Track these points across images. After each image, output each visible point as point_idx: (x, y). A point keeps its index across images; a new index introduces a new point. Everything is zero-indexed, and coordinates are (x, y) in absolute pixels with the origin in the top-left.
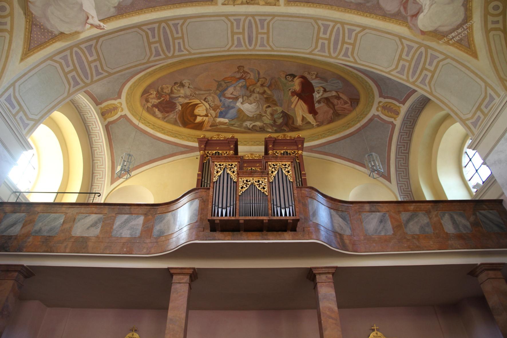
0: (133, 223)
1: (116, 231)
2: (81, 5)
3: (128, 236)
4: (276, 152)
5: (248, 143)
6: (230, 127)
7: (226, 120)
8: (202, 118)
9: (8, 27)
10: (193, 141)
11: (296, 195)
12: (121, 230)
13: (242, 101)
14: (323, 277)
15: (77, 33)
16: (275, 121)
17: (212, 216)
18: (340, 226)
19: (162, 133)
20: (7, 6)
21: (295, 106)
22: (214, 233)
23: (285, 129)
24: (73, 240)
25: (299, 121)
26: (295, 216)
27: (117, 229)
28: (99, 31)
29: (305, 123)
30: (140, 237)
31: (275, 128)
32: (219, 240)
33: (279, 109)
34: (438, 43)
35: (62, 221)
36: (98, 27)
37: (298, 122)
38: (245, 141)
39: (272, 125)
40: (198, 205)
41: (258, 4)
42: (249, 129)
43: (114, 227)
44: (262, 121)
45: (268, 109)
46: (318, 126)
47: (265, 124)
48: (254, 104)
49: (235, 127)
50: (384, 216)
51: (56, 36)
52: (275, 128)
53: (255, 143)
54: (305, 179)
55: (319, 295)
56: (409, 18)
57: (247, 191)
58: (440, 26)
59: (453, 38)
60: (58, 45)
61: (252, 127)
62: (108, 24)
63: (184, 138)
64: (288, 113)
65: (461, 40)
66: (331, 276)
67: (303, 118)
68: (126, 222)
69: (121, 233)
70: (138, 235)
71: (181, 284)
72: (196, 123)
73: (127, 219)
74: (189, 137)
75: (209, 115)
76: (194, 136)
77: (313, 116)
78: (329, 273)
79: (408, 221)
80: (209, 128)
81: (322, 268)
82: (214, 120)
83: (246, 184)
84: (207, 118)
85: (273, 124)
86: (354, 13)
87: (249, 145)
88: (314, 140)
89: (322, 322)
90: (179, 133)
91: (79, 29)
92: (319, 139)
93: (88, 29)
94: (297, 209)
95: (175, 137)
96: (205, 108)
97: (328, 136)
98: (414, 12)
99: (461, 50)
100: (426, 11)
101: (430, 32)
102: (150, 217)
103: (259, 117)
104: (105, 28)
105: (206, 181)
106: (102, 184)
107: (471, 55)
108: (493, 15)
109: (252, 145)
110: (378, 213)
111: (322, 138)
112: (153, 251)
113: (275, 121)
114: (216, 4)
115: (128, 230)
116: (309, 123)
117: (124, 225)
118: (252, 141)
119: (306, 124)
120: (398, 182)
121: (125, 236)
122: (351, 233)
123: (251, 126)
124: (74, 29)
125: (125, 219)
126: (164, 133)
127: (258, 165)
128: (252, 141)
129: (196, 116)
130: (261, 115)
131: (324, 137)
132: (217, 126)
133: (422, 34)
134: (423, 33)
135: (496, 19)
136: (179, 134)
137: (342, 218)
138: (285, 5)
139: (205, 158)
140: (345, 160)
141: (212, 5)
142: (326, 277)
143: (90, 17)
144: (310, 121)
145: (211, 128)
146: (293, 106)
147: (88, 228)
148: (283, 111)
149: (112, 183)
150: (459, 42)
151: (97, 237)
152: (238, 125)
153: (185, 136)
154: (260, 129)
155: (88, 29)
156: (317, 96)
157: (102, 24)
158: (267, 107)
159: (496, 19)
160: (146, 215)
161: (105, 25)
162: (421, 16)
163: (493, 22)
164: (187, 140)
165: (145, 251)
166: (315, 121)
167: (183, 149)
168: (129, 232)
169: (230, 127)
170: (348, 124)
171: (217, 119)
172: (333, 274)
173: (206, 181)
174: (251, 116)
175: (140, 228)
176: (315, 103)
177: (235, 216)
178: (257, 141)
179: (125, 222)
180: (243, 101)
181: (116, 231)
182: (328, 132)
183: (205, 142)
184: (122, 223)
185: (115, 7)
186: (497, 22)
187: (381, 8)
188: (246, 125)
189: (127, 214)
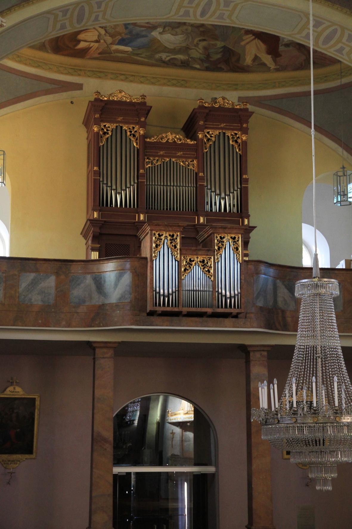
0: (43, 285)
1: (24, 296)
3: (40, 303)
4: (208, 133)
5: (159, 81)
6: (132, 57)
7: (129, 49)
8: (88, 44)
10: (66, 74)
11: (234, 227)
12: (30, 295)
13: (162, 31)
14: (258, 355)
16: (208, 56)
17: (153, 306)
18: (285, 300)
19: (16, 61)
21: (248, 43)
22: (152, 317)
23: (223, 67)
25: (248, 60)
26: (240, 308)
27: (24, 294)
29: (256, 64)
31: (206, 65)
32: (157, 325)
33: (220, 44)
37: (246, 61)
38: (153, 78)
39: (202, 60)
40: (131, 280)
43: (20, 290)
44: (189, 55)
45: (201, 42)
46: (277, 70)
47: (191, 58)
48: (182, 36)
49: (140, 57)
52: (206, 65)
53: (169, 81)
54: (247, 188)
55: (251, 374)
57: (190, 273)
61: (169, 60)
63: (52, 69)
64: (234, 49)
67: (256, 58)
68: (34, 283)
69: (31, 299)
70: (52, 302)
71: (106, 359)
72: (75, 49)
73: (33, 280)
74: (61, 67)
75: (102, 41)
76: (70, 65)
77: (272, 57)
78: (263, 351)
80: (96, 55)
81: (257, 346)
82: (108, 47)
83: (190, 264)
84: (96, 45)
85: (205, 59)
87: (160, 85)
88: (265, 88)
89: (251, 403)
90: (44, 61)
92: (274, 87)
94: (243, 300)
95: (38, 67)
96: (97, 33)
97: (291, 85)
102: (63, 277)
103: (185, 50)
104: (4, 24)
109: (164, 85)
111: (279, 87)
113: (208, 56)
115: (38, 294)
116: (264, 64)
117: (31, 288)
118: (164, 79)
119: (258, 65)
121: (36, 303)
122: (295, 308)
123: (168, 58)
125: (32, 280)
126: (20, 62)
127: (179, 154)
128: (164, 79)
129: (79, 41)
130: (188, 48)
132: (112, 53)
136: (44, 63)
137: (288, 289)
139: (101, 137)
142: (261, 354)
144: (266, 62)
145: (100, 56)
146: (243, 43)
148: (225, 46)
152: (146, 55)
153: (54, 65)
154: (182, 63)
156: (295, 424)
158: (200, 41)
160: (57, 274)
161: (4, 20)
164: (56, 72)
165: (64, 323)
166: (274, 64)
167: (49, 86)
169: (132, 57)
170: (326, 77)
171: (113, 45)
172: (268, 351)
173: (105, 182)
174: (172, 48)
175: (53, 291)
176: (280, 45)
177: (178, 306)
178: (173, 79)
179: (32, 283)
180: (163, 31)
181: (24, 296)
182: (292, 81)
183: (101, 108)
184: (29, 285)
188: (161, 57)
189: (33, 272)
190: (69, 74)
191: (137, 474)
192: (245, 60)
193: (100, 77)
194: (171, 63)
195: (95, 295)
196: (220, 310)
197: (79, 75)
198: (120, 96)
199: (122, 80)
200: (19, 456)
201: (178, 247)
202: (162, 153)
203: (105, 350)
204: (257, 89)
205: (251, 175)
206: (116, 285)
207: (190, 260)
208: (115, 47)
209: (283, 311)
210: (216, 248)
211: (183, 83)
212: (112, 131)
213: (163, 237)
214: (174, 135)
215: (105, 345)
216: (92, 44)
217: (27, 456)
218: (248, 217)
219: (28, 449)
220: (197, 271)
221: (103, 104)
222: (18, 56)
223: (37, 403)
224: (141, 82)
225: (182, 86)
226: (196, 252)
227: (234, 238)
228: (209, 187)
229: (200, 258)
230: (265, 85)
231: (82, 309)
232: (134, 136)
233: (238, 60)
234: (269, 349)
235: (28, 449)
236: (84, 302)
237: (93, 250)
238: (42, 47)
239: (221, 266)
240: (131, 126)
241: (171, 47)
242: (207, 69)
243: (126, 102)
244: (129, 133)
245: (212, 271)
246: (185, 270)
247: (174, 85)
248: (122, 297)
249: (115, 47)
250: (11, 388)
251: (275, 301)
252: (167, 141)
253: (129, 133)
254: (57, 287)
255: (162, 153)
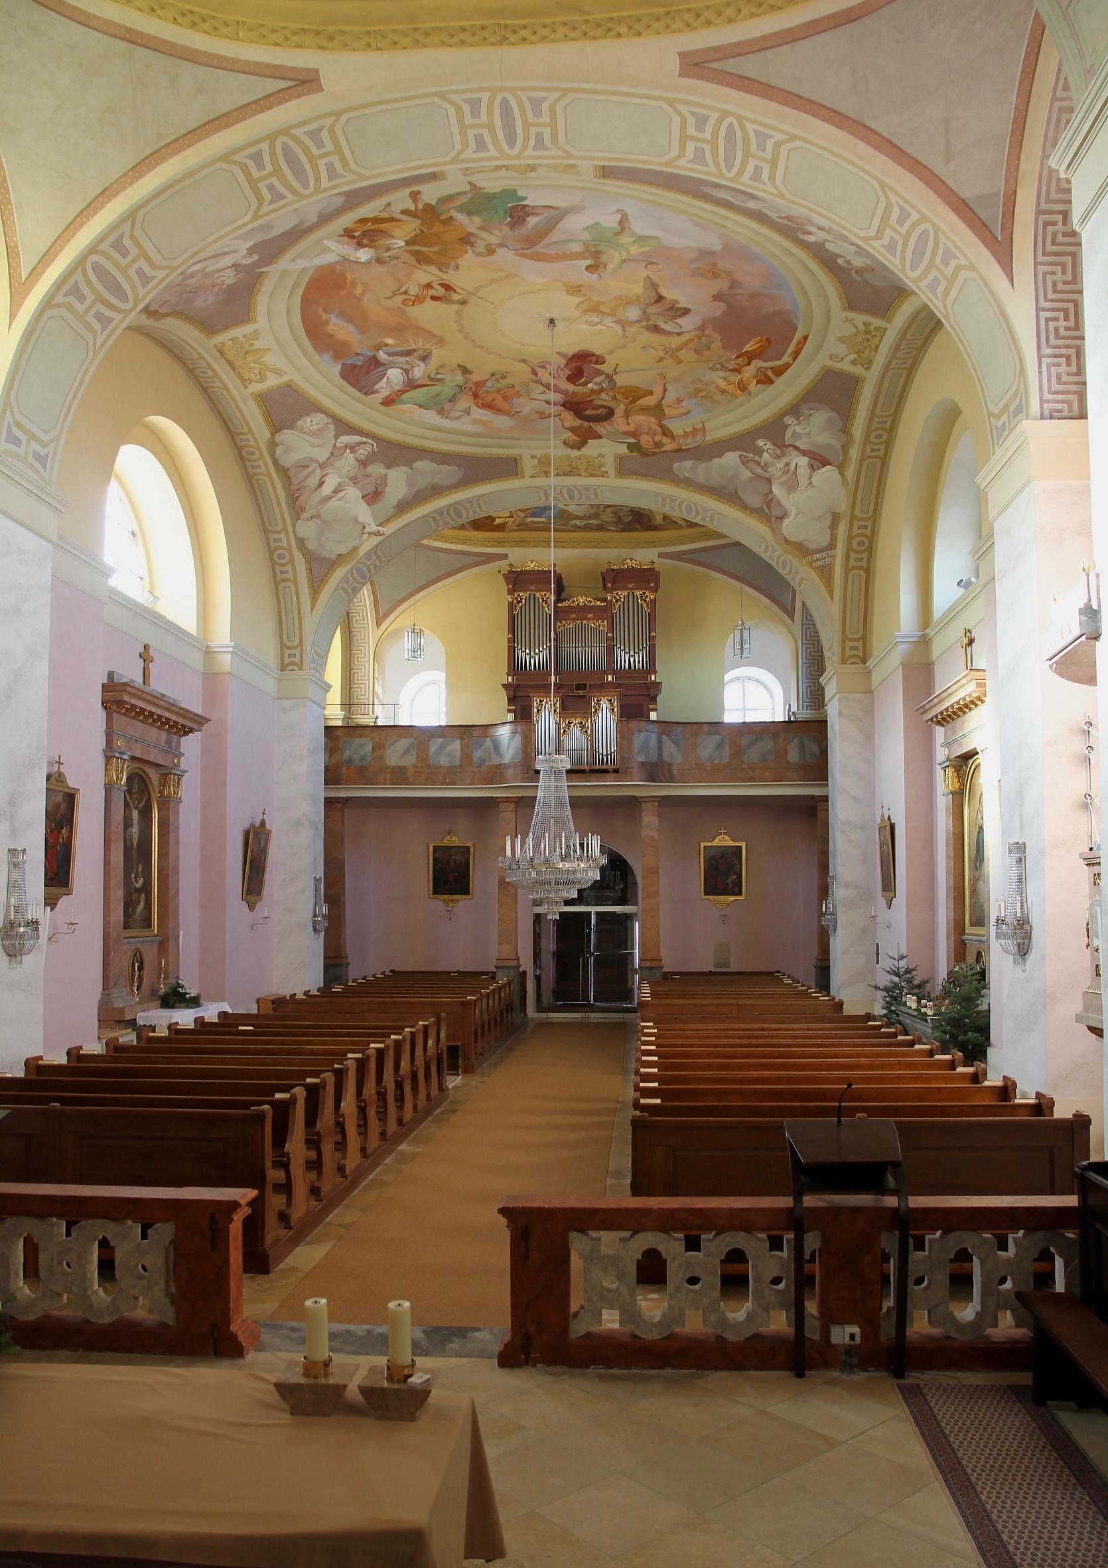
0: (449, 748)
2: (356, 518)
9: (291, 576)
14: (649, 805)
15: (355, 549)
20: (287, 554)
24: (389, 771)
28: (381, 538)
30: (461, 766)
31: (620, 526)
34: (801, 561)
35: (371, 747)
36: (377, 534)
41: (580, 475)
42: (580, 527)
50: (722, 740)
51: (334, 562)
52: (620, 526)
54: (655, 644)
56: (773, 519)
58: (805, 540)
59: (817, 560)
60: (340, 572)
62: (388, 526)
65: (824, 567)
66: (657, 803)
69: (439, 762)
70: (458, 763)
73: (441, 745)
79: (751, 745)
84: (512, 519)
86: (707, 496)
88: (682, 544)
91: (356, 543)
92: (690, 542)
93: (366, 540)
95: (464, 543)
97: (706, 539)
98: (779, 514)
99: (821, 579)
100: (792, 518)
101: (795, 543)
105: (519, 647)
106: (364, 628)
107: (828, 591)
108: (857, 552)
110: (717, 736)
112: (476, 782)
114: (523, 477)
120: (1041, 258)
123: (582, 525)
124: (351, 546)
127: (590, 616)
131: (699, 541)
133: (785, 543)
134: (787, 542)
135: (860, 556)
138: (616, 477)
140: (730, 577)
141: (516, 478)
143: (367, 526)
147: (402, 755)
149: (378, 626)
150: (822, 568)
151: (415, 766)
155: (366, 540)
157: (380, 529)
159: (860, 556)
160: (461, 738)
162: (786, 521)
163: (856, 560)
165: (468, 781)
168: (447, 759)
172: (659, 802)
173: (519, 647)
175: (458, 754)
184: (438, 749)
185: (394, 507)
186: (861, 560)
187: (739, 498)
190: (492, 546)
191: (597, 913)
192: (656, 519)
193: (523, 546)
194: (587, 528)
195: (494, 756)
196: (597, 767)
197: (503, 546)
198: (532, 565)
199: (544, 547)
200: (457, 897)
201: (558, 711)
202: (573, 616)
203: (508, 804)
204: (674, 545)
205: (658, 634)
206: (508, 748)
207: (569, 722)
208: (529, 519)
209: (670, 765)
210: (593, 710)
211: (603, 545)
212: (525, 600)
213: (544, 703)
214: (584, 598)
215: (507, 800)
216: (507, 520)
217: (464, 897)
218: (655, 673)
219: (466, 891)
220: (576, 731)
221: (515, 575)
222: (443, 537)
223: (472, 850)
224: (564, 547)
225: (602, 547)
226: (574, 716)
227: (611, 700)
228: (618, 646)
229: (578, 720)
230: (681, 541)
231: (484, 769)
232: (546, 602)
233: (650, 520)
234: (659, 799)
235: (466, 891)
236: (485, 762)
237: (509, 711)
238: (462, 527)
239: (598, 725)
240: (543, 593)
241: (582, 515)
242: (623, 530)
243: (538, 570)
244: (541, 600)
245: (589, 732)
246: (564, 731)
247: (594, 547)
248: (514, 757)
249: (529, 519)
250: (448, 838)
251: (660, 755)
252: (578, 605)
253: (541, 600)
254: (462, 749)
255: (573, 616)
